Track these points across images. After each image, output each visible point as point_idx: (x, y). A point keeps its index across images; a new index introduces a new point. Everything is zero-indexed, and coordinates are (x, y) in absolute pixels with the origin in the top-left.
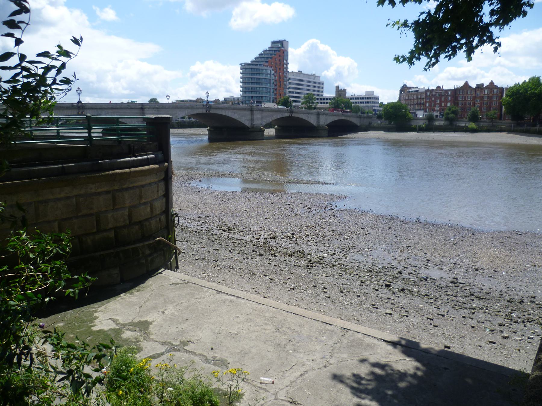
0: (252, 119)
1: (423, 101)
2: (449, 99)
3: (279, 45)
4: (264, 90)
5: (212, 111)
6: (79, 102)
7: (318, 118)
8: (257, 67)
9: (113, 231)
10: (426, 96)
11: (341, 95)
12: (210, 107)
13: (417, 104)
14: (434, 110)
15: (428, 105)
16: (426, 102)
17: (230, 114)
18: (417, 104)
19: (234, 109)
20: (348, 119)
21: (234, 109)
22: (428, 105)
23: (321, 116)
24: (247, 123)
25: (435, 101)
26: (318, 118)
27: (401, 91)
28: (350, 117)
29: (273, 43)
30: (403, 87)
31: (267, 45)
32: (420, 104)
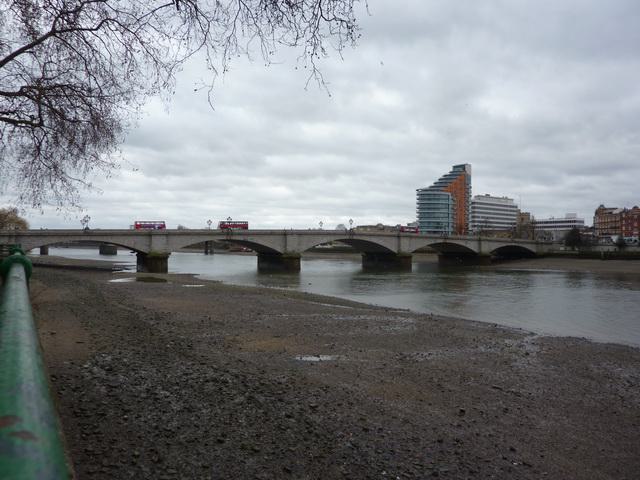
0: (399, 246)
1: (618, 225)
2: (636, 224)
3: (461, 169)
4: (442, 215)
5: (355, 237)
6: (87, 228)
7: (480, 244)
8: (436, 193)
9: (254, 285)
10: (622, 219)
11: (522, 219)
12: (354, 234)
13: (611, 228)
14: (632, 235)
15: (624, 228)
16: (622, 225)
17: (374, 240)
18: (611, 228)
19: (379, 235)
20: (520, 245)
21: (379, 235)
22: (624, 228)
23: (483, 243)
24: (394, 249)
25: (632, 224)
26: (480, 244)
27: (596, 213)
28: (522, 243)
29: (454, 167)
30: (599, 209)
31: (447, 170)
32: (615, 228)
